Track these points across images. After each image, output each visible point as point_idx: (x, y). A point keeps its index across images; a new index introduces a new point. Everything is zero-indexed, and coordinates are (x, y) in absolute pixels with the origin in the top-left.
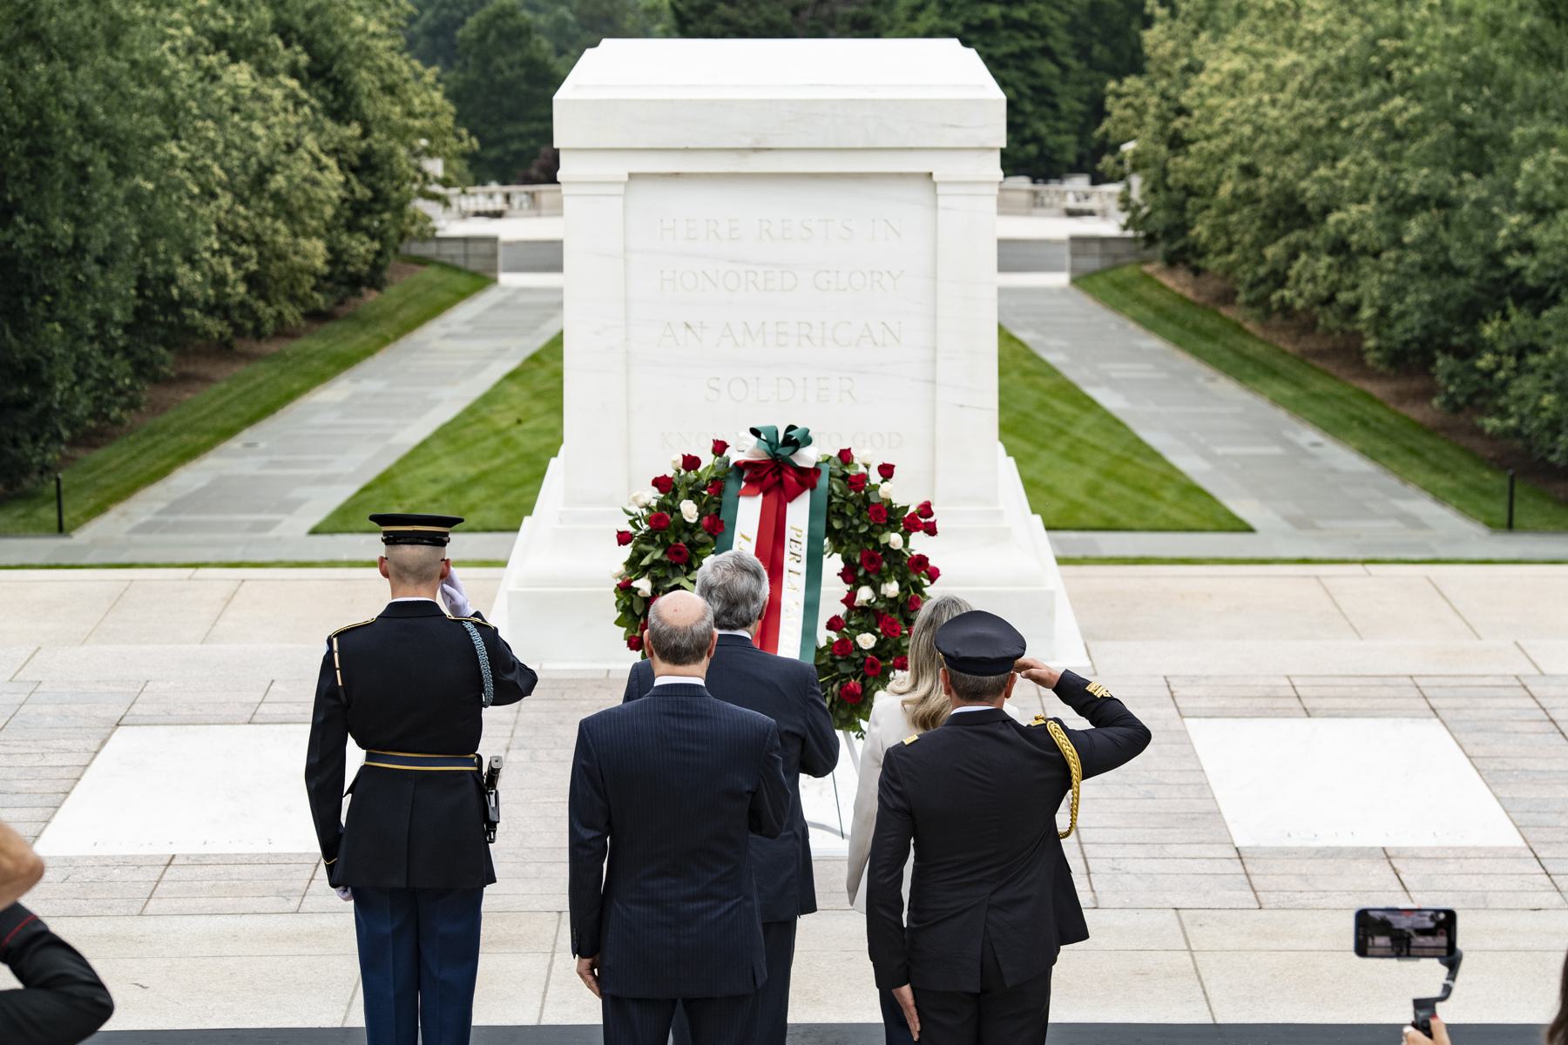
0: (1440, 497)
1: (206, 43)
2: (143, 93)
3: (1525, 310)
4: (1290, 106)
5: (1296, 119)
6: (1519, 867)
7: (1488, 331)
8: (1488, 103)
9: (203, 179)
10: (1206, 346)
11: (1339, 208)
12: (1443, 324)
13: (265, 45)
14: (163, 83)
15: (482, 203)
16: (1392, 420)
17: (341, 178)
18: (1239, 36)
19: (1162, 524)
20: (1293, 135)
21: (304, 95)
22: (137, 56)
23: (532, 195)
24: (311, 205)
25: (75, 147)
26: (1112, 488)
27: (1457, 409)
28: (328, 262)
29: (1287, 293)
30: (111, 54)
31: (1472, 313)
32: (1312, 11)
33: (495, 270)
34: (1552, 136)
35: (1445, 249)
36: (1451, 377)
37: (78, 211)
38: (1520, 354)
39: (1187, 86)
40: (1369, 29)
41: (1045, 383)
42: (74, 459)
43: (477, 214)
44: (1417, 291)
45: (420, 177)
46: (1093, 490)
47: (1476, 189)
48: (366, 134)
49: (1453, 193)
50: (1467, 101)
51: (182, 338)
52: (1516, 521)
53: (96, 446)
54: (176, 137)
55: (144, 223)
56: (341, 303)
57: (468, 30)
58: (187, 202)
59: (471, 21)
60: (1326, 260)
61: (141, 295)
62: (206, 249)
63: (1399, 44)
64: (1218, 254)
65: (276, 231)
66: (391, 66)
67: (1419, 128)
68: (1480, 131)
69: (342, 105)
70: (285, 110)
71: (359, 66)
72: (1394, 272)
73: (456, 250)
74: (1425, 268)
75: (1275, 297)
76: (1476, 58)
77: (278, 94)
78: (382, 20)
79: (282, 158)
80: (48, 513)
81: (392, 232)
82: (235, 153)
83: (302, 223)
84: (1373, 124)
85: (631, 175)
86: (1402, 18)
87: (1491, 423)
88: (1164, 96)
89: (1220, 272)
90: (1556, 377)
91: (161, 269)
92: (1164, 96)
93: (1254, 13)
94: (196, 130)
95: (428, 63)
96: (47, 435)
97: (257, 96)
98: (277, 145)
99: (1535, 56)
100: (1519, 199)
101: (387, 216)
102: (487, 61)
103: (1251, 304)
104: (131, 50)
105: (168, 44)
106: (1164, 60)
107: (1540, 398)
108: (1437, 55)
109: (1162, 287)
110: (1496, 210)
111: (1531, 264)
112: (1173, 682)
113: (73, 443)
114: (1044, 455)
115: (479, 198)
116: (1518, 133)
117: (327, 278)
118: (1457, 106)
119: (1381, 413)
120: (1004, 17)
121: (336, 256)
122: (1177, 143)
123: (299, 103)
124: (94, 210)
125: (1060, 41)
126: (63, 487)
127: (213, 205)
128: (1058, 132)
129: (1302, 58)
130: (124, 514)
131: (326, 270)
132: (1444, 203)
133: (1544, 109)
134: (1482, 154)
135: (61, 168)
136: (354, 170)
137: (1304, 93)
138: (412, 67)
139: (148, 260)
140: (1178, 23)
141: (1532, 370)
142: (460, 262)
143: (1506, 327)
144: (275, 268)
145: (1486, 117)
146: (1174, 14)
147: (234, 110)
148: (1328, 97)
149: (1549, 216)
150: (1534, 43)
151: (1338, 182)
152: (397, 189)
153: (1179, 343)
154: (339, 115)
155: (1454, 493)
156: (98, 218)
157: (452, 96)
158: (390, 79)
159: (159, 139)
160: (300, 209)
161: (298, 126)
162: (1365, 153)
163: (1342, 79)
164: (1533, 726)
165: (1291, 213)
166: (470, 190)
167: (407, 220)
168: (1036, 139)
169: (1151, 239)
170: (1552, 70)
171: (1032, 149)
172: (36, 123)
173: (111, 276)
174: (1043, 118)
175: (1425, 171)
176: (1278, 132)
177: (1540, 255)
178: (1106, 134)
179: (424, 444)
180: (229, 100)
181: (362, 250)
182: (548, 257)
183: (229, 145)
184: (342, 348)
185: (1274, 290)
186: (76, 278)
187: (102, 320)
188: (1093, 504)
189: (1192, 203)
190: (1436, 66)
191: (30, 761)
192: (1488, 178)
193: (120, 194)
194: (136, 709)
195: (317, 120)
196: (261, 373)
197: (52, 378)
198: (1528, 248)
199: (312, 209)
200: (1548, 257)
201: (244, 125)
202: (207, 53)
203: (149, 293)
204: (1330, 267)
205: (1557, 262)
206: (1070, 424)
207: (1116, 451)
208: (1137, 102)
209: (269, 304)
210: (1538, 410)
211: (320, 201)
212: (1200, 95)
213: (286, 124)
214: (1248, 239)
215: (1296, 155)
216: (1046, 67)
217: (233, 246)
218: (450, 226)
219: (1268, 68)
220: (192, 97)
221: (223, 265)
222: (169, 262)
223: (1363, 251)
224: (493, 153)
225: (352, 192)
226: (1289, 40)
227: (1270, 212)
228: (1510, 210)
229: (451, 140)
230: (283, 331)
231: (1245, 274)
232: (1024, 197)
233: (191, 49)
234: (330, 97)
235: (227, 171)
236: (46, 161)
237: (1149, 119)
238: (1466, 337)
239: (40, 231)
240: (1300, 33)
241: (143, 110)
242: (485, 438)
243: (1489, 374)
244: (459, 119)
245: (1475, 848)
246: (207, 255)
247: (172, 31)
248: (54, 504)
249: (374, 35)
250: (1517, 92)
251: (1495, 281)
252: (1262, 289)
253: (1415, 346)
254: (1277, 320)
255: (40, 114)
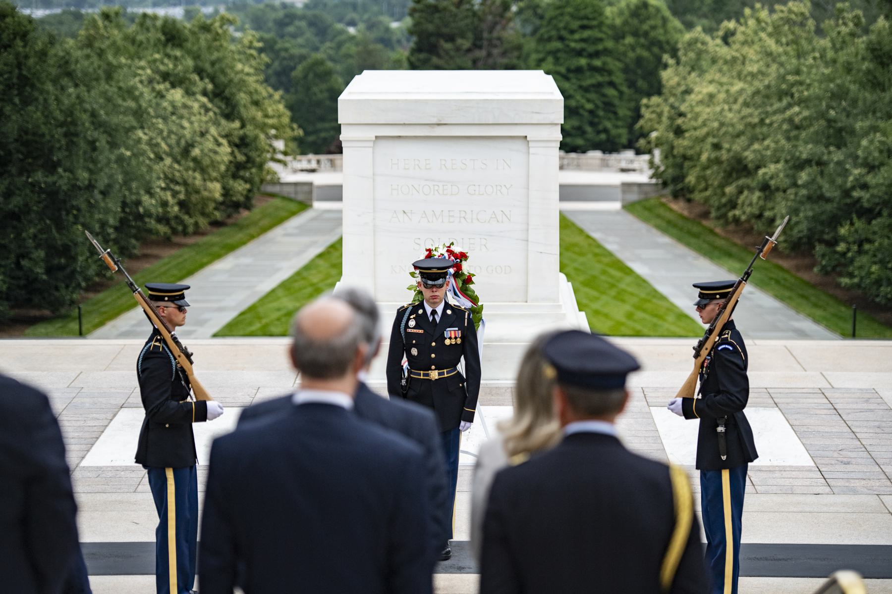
0: (817, 321)
1: (158, 77)
2: (125, 104)
3: (863, 220)
4: (739, 112)
5: (743, 118)
6: (811, 475)
7: (843, 231)
8: (844, 109)
9: (156, 149)
10: (693, 240)
11: (765, 167)
12: (819, 228)
13: (189, 80)
14: (136, 99)
15: (304, 165)
16: (793, 280)
17: (229, 150)
18: (712, 74)
19: (666, 333)
20: (740, 127)
21: (210, 105)
22: (122, 84)
23: (331, 161)
24: (214, 164)
25: (89, 133)
26: (640, 315)
27: (827, 273)
28: (223, 195)
29: (737, 212)
30: (107, 83)
31: (834, 221)
32: (751, 60)
33: (311, 200)
34: (878, 127)
35: (820, 188)
36: (823, 256)
37: (91, 166)
38: (860, 245)
39: (684, 101)
40: (782, 71)
41: (605, 260)
42: (87, 298)
43: (302, 170)
44: (805, 210)
45: (271, 150)
46: (630, 316)
47: (838, 156)
48: (243, 126)
49: (825, 158)
50: (833, 108)
51: (146, 237)
52: (857, 333)
53: (99, 291)
54: (142, 128)
55: (126, 173)
56: (229, 216)
57: (298, 72)
58: (147, 162)
59: (300, 68)
60: (757, 194)
61: (123, 211)
62: (158, 187)
63: (797, 78)
64: (701, 191)
65: (194, 178)
66: (256, 91)
67: (809, 121)
68: (839, 125)
69: (230, 112)
70: (200, 114)
71: (239, 90)
72: (794, 200)
73: (290, 189)
74: (809, 198)
75: (730, 214)
76: (838, 85)
77: (196, 106)
78: (251, 66)
79: (198, 139)
80: (74, 326)
81: (257, 179)
82: (173, 136)
83: (209, 175)
84: (784, 121)
85: (376, 137)
86: (800, 64)
87: (845, 281)
88: (672, 107)
89: (702, 201)
90: (880, 256)
91: (134, 197)
92: (672, 107)
93: (721, 62)
94: (153, 124)
95: (276, 89)
96: (74, 285)
97: (185, 106)
98: (195, 132)
99: (870, 85)
100: (860, 161)
101: (254, 170)
102: (308, 89)
103: (718, 218)
104: (118, 81)
105: (137, 79)
106: (673, 87)
107: (870, 267)
108: (816, 84)
109: (671, 210)
110: (848, 166)
111: (864, 195)
112: (645, 390)
113: (87, 289)
114: (604, 298)
115: (304, 162)
116: (858, 125)
117: (222, 203)
118: (827, 111)
119: (787, 276)
120: (589, 65)
121: (226, 192)
122: (679, 132)
123: (207, 110)
124: (99, 166)
125: (619, 78)
126: (83, 312)
127: (161, 164)
128: (617, 127)
129: (746, 86)
130: (114, 326)
131: (221, 199)
132: (820, 163)
133: (874, 112)
134: (842, 137)
135: (83, 144)
136: (237, 146)
137: (746, 104)
138: (268, 92)
139: (127, 193)
140: (681, 68)
141: (866, 252)
142: (293, 196)
143: (852, 229)
144: (194, 198)
145: (844, 118)
146: (678, 63)
147: (173, 114)
148: (760, 106)
149: (876, 170)
150: (870, 77)
151: (764, 153)
152: (259, 156)
153: (680, 239)
154: (229, 117)
155: (825, 318)
156: (101, 170)
157: (290, 107)
158: (255, 97)
159: (133, 128)
160: (207, 166)
161: (207, 122)
162: (779, 136)
163: (767, 97)
164: (826, 412)
165: (740, 168)
166: (299, 157)
167: (264, 173)
168: (606, 131)
169: (665, 184)
170: (879, 92)
171: (603, 136)
172: (69, 119)
173: (107, 200)
174: (609, 119)
175: (810, 146)
176: (733, 125)
177: (871, 191)
178: (641, 127)
179: (273, 291)
180: (170, 109)
181: (240, 188)
182: (335, 193)
183: (170, 132)
184: (230, 241)
185: (730, 210)
186: (89, 202)
187: (103, 224)
188: (630, 323)
189: (687, 164)
190: (816, 90)
191: (79, 424)
192: (844, 149)
193: (113, 157)
194: (130, 400)
195: (216, 119)
196: (186, 254)
197: (77, 254)
198: (865, 187)
199: (214, 167)
200: (875, 191)
201: (177, 121)
202: (158, 83)
203: (128, 210)
204: (759, 198)
205: (880, 194)
206: (618, 281)
207: (643, 295)
208: (658, 110)
209: (191, 217)
210: (870, 273)
211: (218, 163)
212: (691, 106)
213: (200, 121)
214: (716, 183)
215: (743, 138)
216: (611, 92)
217: (172, 186)
218: (287, 176)
219: (727, 91)
220: (151, 106)
221: (166, 196)
222: (138, 194)
223: (778, 189)
224: (311, 138)
225: (235, 157)
226: (739, 76)
227: (728, 169)
228: (856, 166)
229: (288, 130)
230: (198, 232)
231: (714, 201)
232: (598, 162)
233: (151, 81)
234: (223, 107)
235: (169, 146)
236: (75, 139)
237: (665, 119)
238: (832, 235)
239: (71, 176)
240: (745, 72)
241: (124, 113)
242: (305, 288)
243: (844, 254)
244: (293, 120)
245: (789, 466)
246: (158, 190)
247: (140, 72)
248: (77, 321)
249: (248, 74)
250: (860, 103)
251: (847, 204)
252: (723, 210)
253: (805, 240)
254: (731, 227)
255: (71, 114)
